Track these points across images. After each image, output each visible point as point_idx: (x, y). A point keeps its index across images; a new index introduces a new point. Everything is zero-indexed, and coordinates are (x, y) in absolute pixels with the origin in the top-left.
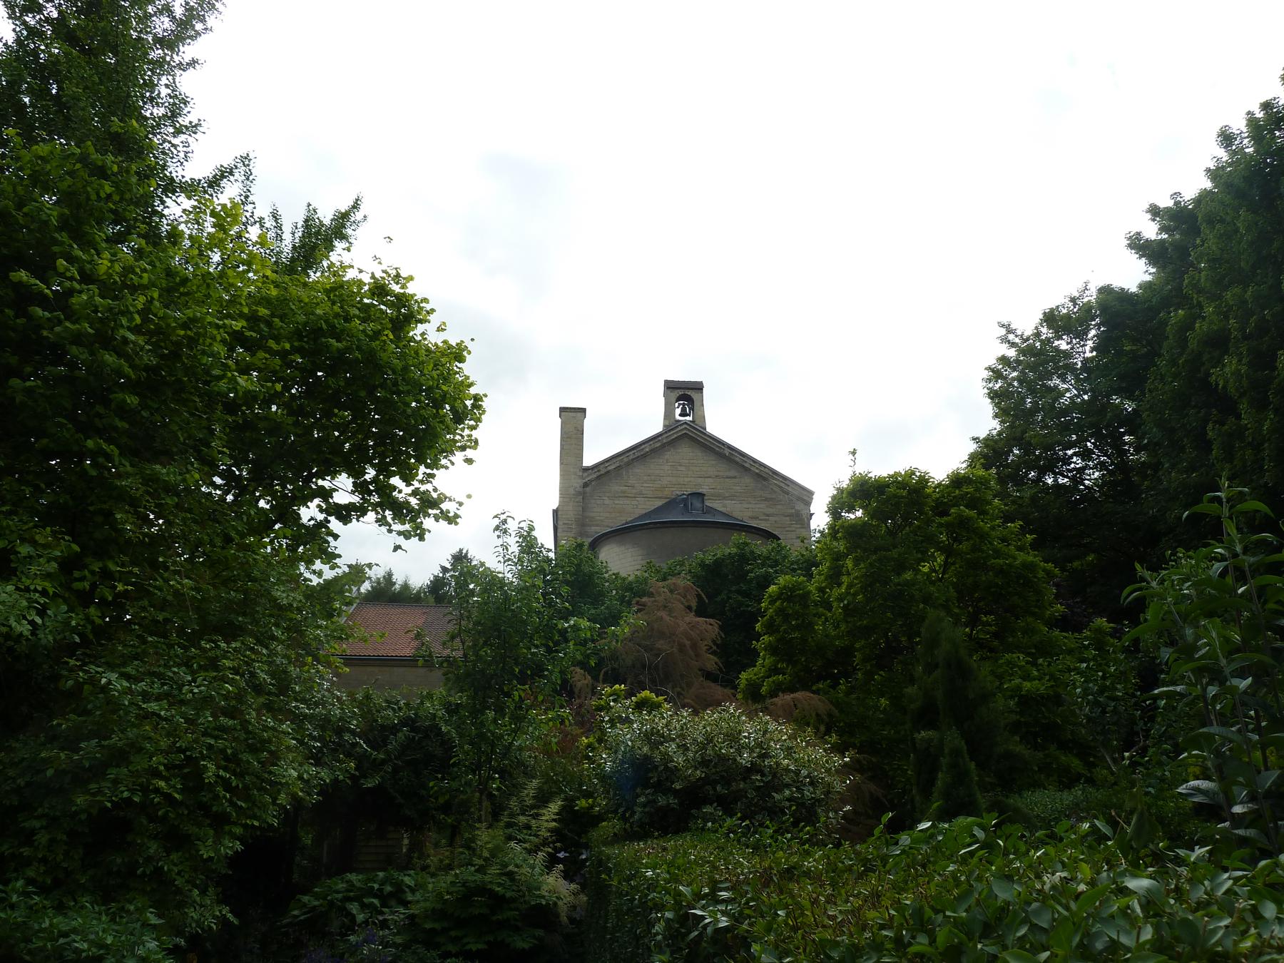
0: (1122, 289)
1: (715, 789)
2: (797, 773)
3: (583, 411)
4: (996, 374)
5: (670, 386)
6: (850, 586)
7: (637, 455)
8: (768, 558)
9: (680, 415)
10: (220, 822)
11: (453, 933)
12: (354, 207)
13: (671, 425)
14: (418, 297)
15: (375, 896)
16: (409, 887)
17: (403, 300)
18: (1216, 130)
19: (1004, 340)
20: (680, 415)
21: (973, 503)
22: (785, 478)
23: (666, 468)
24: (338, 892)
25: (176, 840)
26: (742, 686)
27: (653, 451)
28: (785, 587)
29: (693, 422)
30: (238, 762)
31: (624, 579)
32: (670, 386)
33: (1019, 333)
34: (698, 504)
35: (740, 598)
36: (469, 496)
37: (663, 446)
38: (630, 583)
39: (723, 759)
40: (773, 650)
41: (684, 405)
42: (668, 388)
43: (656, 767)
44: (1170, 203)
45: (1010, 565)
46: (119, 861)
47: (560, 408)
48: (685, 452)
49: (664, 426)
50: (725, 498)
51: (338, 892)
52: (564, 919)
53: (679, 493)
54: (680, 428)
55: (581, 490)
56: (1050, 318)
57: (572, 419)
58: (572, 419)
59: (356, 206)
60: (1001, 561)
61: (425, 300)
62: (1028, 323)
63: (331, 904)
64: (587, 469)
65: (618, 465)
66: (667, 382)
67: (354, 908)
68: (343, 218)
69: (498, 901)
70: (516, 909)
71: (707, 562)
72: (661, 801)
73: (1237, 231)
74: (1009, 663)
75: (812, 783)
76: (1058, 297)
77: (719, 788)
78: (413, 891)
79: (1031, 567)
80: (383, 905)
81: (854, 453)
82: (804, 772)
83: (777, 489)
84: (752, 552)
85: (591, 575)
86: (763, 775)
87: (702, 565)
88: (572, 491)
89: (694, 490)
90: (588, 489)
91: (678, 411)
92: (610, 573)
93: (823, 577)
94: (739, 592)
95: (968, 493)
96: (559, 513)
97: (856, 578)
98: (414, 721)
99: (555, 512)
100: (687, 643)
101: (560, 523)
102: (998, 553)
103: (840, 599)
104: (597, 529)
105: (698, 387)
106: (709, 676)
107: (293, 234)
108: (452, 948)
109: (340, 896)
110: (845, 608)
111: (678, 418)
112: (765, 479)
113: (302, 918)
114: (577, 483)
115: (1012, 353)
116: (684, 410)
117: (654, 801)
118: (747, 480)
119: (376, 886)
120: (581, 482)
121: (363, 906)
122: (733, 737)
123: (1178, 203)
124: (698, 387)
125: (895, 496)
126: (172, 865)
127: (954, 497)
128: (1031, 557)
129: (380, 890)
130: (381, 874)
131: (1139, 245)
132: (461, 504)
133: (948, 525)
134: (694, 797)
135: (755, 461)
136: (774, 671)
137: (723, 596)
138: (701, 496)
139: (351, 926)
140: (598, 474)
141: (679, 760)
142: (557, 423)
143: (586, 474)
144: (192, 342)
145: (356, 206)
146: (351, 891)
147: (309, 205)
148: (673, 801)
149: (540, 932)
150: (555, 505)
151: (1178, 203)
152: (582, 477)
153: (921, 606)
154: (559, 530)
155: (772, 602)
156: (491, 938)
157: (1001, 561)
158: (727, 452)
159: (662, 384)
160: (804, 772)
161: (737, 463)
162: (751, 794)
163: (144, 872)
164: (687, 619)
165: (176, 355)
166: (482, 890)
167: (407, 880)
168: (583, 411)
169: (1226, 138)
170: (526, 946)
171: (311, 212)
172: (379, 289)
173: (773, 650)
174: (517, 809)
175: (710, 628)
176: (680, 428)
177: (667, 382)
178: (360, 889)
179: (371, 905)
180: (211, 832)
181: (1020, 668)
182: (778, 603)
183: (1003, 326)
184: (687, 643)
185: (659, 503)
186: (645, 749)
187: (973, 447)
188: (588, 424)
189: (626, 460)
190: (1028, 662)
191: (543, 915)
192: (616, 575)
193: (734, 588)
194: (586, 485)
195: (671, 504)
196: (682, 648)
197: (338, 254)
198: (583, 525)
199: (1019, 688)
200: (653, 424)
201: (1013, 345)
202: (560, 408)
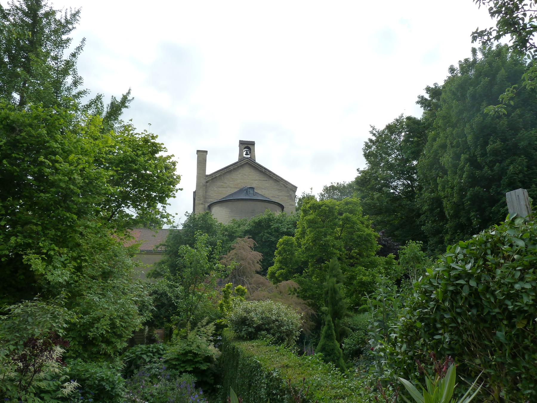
0: (415, 118)
1: (265, 326)
2: (288, 321)
3: (206, 152)
4: (368, 146)
5: (242, 143)
6: (308, 240)
7: (228, 170)
8: (279, 220)
9: (245, 155)
10: (120, 336)
11: (182, 365)
12: (129, 93)
13: (241, 159)
14: (160, 143)
15: (151, 353)
16: (161, 349)
17: (154, 145)
18: (449, 67)
19: (371, 132)
20: (245, 155)
21: (351, 212)
22: (286, 182)
23: (239, 176)
24: (138, 351)
25: (108, 342)
26: (269, 273)
27: (234, 169)
28: (285, 240)
29: (250, 158)
30: (124, 319)
31: (224, 227)
32: (242, 143)
33: (377, 130)
34: (251, 192)
35: (268, 235)
36: (177, 214)
37: (238, 167)
38: (226, 228)
39: (267, 317)
40: (281, 262)
41: (247, 150)
42: (241, 144)
43: (248, 319)
44: (434, 87)
45: (362, 234)
46: (95, 350)
47: (197, 151)
48: (247, 171)
49: (239, 159)
50: (262, 189)
51: (138, 351)
52: (215, 359)
53: (245, 186)
54: (245, 160)
55: (205, 184)
56: (389, 127)
57: (202, 155)
58: (202, 155)
59: (129, 93)
60: (359, 233)
61: (163, 144)
62: (381, 127)
63: (137, 356)
64: (207, 176)
65: (220, 174)
66: (240, 141)
67: (144, 356)
68: (125, 99)
69: (196, 355)
70: (201, 357)
71: (256, 221)
72: (250, 330)
73: (452, 107)
74: (359, 270)
75: (292, 324)
76: (390, 120)
77: (266, 326)
78: (163, 350)
79: (369, 235)
80: (154, 355)
81: (311, 189)
82: (290, 321)
83: (282, 185)
84: (273, 218)
85: (211, 224)
86: (279, 322)
87: (254, 222)
88: (201, 184)
89: (250, 186)
90: (208, 184)
91: (245, 153)
92: (218, 223)
93: (298, 234)
94: (268, 233)
95: (350, 208)
96: (196, 193)
97: (310, 237)
98: (157, 291)
99: (194, 193)
100: (251, 262)
101: (196, 197)
102: (359, 230)
103: (304, 245)
104: (211, 200)
105: (253, 144)
106: (257, 272)
107: (107, 108)
108: (182, 370)
109: (139, 353)
110: (306, 248)
111: (245, 156)
112: (278, 182)
113: (128, 360)
114: (204, 181)
115: (374, 138)
116: (247, 152)
117: (247, 330)
118: (271, 182)
119: (151, 349)
120: (205, 181)
121: (147, 356)
122: (270, 311)
123: (436, 87)
124: (253, 144)
125: (324, 210)
126: (110, 350)
127: (345, 209)
128: (369, 231)
129: (152, 351)
130: (152, 345)
131: (422, 102)
132: (174, 217)
133: (343, 219)
134: (259, 328)
135: (274, 174)
136: (281, 268)
137: (262, 234)
138: (253, 188)
139: (145, 363)
140: (212, 178)
141: (255, 319)
142: (196, 156)
143: (207, 178)
144: (97, 179)
145: (129, 93)
146: (142, 351)
147: (113, 96)
148: (253, 330)
149: (209, 364)
150: (194, 189)
151: (436, 87)
152: (205, 179)
153: (332, 248)
154: (196, 200)
155: (280, 245)
156: (194, 366)
157: (359, 233)
158: (263, 170)
159: (238, 143)
160: (290, 321)
161: (267, 175)
162: (275, 327)
163: (102, 353)
164: (252, 253)
165: (91, 183)
166: (190, 352)
167: (161, 347)
168: (206, 152)
169: (452, 70)
170: (205, 368)
171: (114, 98)
172: (146, 141)
173: (281, 262)
174: (200, 326)
175: (258, 256)
176: (245, 160)
177: (240, 141)
178: (145, 350)
179: (150, 356)
180: (119, 340)
181: (363, 272)
182: (282, 246)
183: (372, 127)
184: (251, 262)
185: (236, 190)
186: (245, 315)
187: (357, 174)
188: (208, 157)
189: (223, 172)
190: (365, 270)
191: (208, 359)
192: (221, 224)
193: (266, 231)
194: (207, 182)
195: (241, 191)
196: (249, 263)
197: (125, 117)
198: (206, 198)
199: (362, 279)
200: (235, 159)
201: (374, 135)
202: (197, 151)
